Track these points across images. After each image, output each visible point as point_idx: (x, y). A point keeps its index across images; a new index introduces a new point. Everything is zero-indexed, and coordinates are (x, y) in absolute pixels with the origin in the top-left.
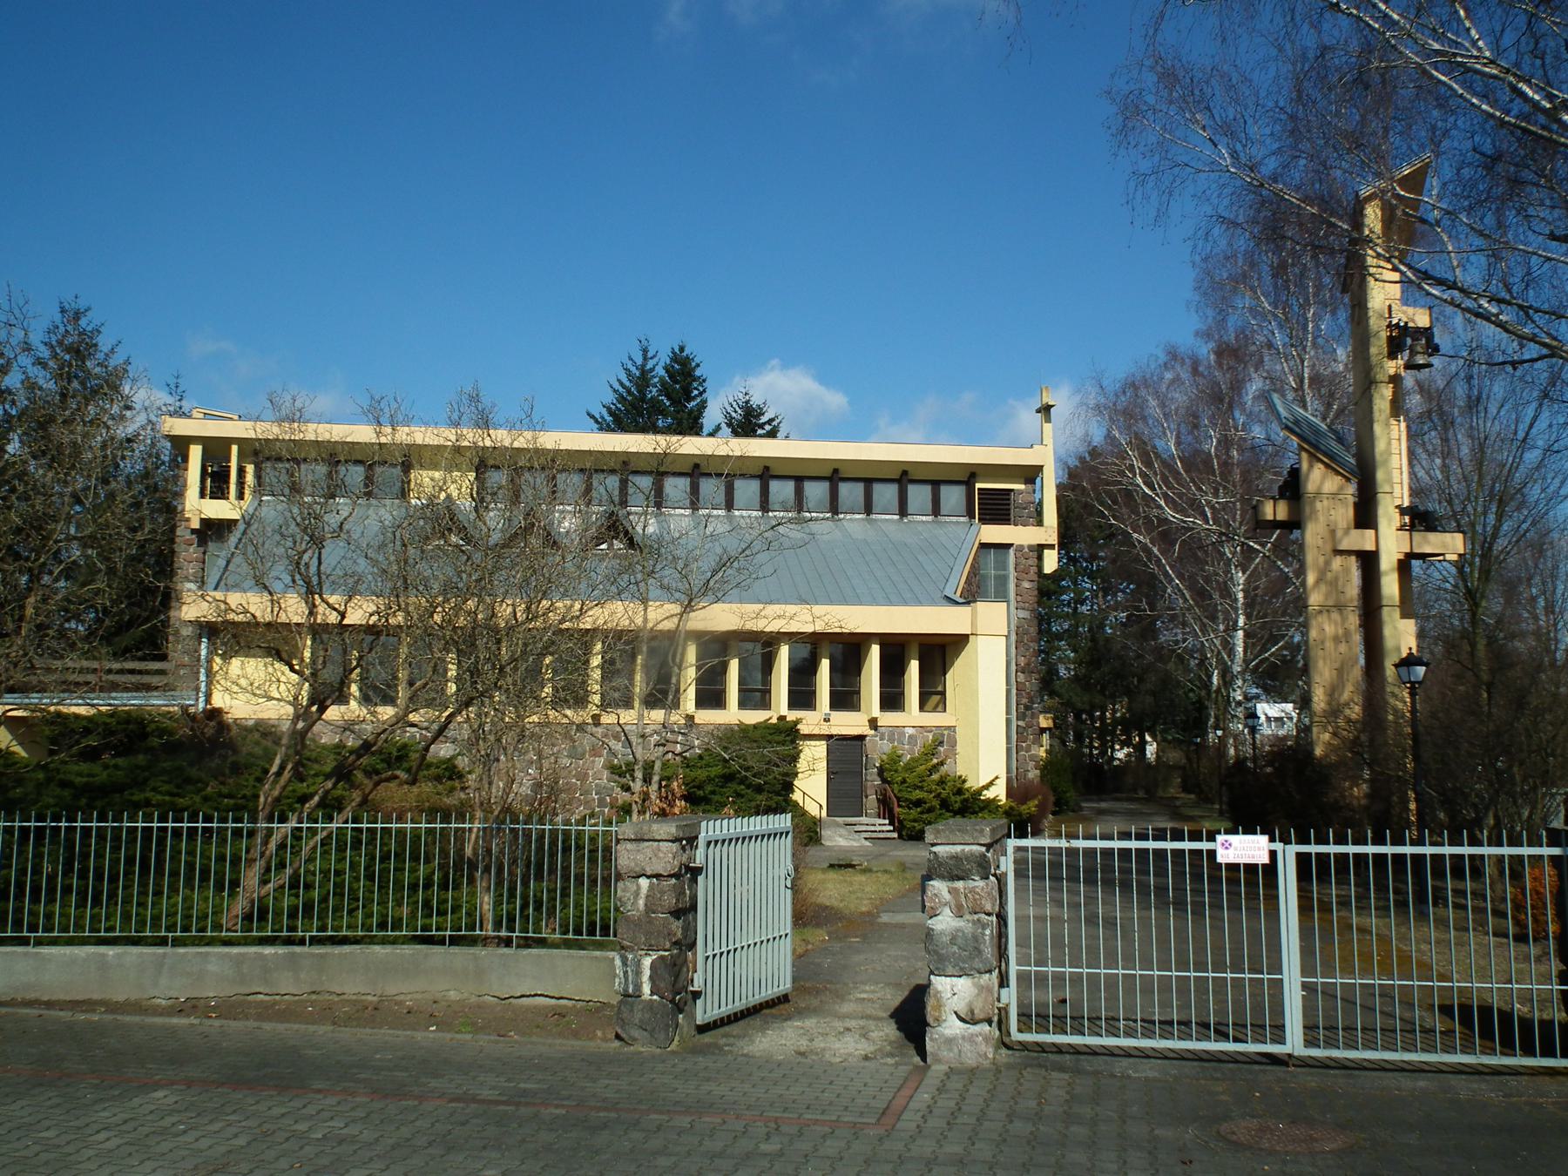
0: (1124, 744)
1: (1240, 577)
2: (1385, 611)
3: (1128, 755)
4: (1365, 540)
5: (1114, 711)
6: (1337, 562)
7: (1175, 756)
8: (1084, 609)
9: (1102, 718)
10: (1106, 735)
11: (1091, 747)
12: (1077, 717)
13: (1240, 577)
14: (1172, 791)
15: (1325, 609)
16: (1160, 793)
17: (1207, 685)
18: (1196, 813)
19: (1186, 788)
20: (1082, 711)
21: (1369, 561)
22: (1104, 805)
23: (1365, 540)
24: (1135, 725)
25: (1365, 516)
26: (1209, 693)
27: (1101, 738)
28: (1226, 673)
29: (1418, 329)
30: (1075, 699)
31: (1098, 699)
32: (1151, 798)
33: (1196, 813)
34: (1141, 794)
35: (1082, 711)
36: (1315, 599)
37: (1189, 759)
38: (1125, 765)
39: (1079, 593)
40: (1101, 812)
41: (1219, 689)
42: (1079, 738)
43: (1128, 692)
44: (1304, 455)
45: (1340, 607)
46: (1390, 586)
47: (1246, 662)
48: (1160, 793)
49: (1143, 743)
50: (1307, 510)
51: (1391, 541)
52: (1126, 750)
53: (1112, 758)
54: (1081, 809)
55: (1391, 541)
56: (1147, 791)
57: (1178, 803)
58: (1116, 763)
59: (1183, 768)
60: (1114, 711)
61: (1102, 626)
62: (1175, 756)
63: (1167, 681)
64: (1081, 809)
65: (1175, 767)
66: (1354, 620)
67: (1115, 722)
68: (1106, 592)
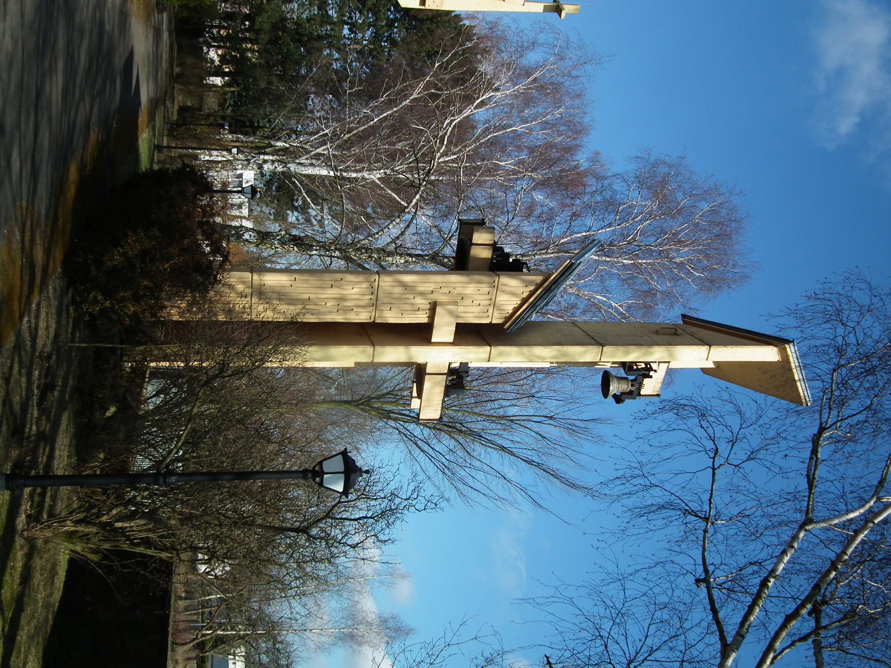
0: (222, 58)
1: (375, 176)
2: (369, 349)
3: (212, 61)
4: (444, 331)
5: (252, 51)
6: (422, 303)
7: (211, 102)
8: (346, 31)
9: (245, 40)
10: (232, 42)
11: (220, 27)
12: (247, 17)
13: (375, 176)
14: (180, 99)
15: (374, 291)
16: (177, 86)
17: (275, 136)
18: (158, 122)
19: (183, 110)
20: (252, 21)
21: (421, 333)
22: (165, 36)
23: (444, 331)
24: (239, 69)
25: (468, 333)
26: (268, 138)
27: (229, 37)
28: (290, 154)
29: (641, 385)
30: (265, 16)
31: (265, 37)
32: (173, 78)
33: (158, 122)
34: (177, 70)
35: (252, 21)
36: (386, 282)
37: (208, 116)
38: (203, 58)
39: (362, 28)
40: (157, 32)
41: (272, 146)
42: (229, 17)
43: (269, 67)
44: (539, 279)
45: (375, 304)
46: (393, 354)
47: (296, 175)
48: (177, 86)
49: (222, 74)
50: (477, 277)
51: (439, 356)
52: (216, 59)
53: (210, 46)
54: (160, 12)
55: (439, 356)
56: (179, 76)
57: (168, 103)
58: (205, 49)
59: (200, 109)
60: (252, 51)
61: (330, 46)
62: (211, 102)
63: (278, 101)
64: (160, 12)
65: (201, 99)
66: (363, 317)
67: (243, 51)
68: (360, 53)
